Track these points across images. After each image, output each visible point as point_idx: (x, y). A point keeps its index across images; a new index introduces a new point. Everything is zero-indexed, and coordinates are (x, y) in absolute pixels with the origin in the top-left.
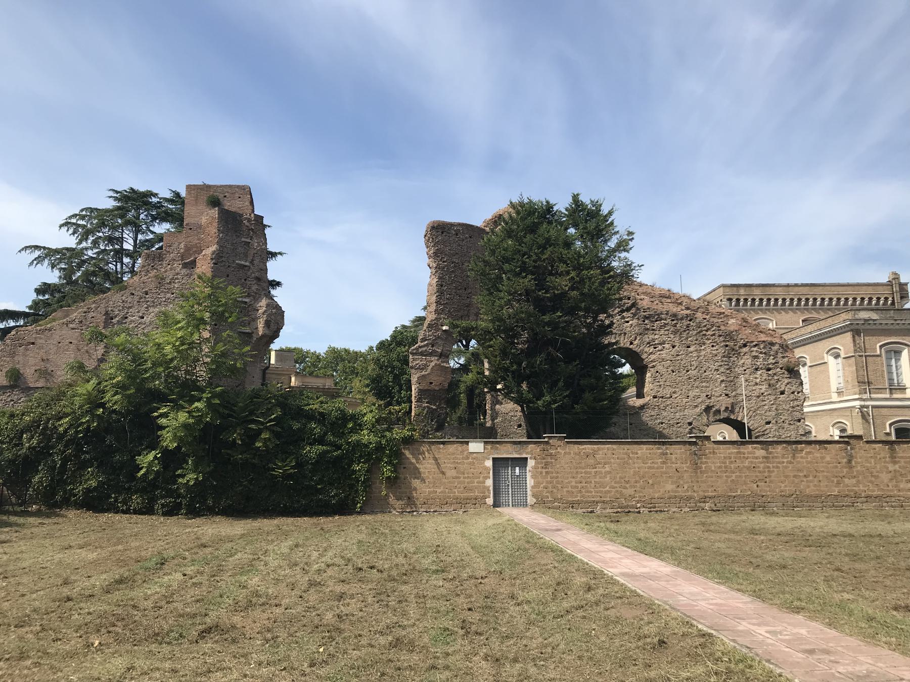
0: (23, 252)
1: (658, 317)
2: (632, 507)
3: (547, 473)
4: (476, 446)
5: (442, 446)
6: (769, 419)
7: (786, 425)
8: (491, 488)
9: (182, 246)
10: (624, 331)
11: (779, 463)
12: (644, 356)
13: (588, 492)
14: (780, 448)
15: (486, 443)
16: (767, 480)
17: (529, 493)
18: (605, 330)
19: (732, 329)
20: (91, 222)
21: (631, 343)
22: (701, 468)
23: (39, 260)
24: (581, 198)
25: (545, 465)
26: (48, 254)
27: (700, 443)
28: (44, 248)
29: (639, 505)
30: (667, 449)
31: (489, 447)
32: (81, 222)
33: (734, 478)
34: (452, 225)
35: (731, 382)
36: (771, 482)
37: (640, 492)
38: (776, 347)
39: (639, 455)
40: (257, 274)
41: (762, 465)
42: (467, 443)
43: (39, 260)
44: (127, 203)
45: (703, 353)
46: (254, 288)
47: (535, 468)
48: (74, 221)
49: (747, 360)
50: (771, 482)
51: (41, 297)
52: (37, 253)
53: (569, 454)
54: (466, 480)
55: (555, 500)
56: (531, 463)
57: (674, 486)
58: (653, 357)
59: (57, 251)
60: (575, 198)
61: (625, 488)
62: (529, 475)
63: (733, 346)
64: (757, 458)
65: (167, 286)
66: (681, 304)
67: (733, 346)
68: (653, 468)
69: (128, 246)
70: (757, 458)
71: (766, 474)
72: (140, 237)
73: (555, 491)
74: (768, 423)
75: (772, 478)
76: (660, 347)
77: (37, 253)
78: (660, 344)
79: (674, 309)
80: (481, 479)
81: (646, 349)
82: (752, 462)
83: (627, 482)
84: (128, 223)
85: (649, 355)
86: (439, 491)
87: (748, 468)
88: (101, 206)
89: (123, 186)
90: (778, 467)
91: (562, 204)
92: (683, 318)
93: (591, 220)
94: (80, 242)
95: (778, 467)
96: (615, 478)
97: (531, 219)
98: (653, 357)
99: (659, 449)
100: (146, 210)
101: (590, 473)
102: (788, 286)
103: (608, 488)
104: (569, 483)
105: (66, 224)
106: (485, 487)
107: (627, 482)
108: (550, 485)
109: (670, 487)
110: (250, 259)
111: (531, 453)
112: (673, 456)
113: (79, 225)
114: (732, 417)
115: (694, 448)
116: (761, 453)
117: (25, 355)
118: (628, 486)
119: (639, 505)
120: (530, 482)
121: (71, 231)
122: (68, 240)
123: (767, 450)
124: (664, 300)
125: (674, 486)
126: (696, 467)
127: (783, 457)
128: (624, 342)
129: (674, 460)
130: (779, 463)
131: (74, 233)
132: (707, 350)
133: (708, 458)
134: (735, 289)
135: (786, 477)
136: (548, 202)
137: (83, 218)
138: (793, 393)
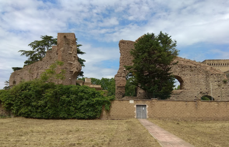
0: (19, 52)
1: (185, 67)
2: (177, 119)
3: (152, 109)
4: (132, 102)
5: (122, 101)
6: (219, 96)
7: (224, 97)
8: (136, 113)
9: (57, 49)
10: (174, 70)
11: (222, 107)
12: (182, 78)
13: (164, 115)
14: (222, 103)
15: (134, 100)
16: (218, 112)
17: (147, 115)
18: (169, 69)
19: (208, 70)
20: (35, 45)
21: (178, 74)
22: (198, 109)
23: (23, 54)
24: (162, 32)
25: (151, 107)
26: (26, 53)
27: (197, 101)
28: (25, 51)
29: (179, 119)
30: (187, 103)
31: (135, 102)
32: (34, 44)
33: (208, 112)
34: (126, 41)
35: (208, 85)
36: (219, 113)
37: (179, 115)
38: (221, 75)
39: (179, 105)
40: (74, 55)
41: (217, 108)
42: (129, 100)
43: (23, 54)
44: (45, 39)
45: (199, 77)
46: (74, 59)
47: (148, 108)
48: (32, 44)
49: (211, 79)
50: (219, 113)
51: (26, 64)
52: (23, 52)
53: (158, 104)
54: (129, 111)
55: (155, 117)
56: (147, 106)
57: (190, 114)
58: (184, 78)
59: (28, 52)
60: (161, 32)
61: (175, 114)
62: (147, 110)
63: (208, 75)
64: (215, 106)
65: (53, 59)
66: (192, 63)
67: (208, 75)
68: (183, 108)
69: (46, 51)
70: (215, 106)
71: (218, 111)
72: (49, 48)
73: (154, 114)
74: (219, 97)
75: (220, 112)
76: (187, 75)
77: (23, 52)
78: (187, 74)
79: (190, 65)
80: (133, 111)
81: (183, 76)
82: (214, 107)
83: (176, 112)
84: (46, 45)
85: (183, 78)
86: (121, 114)
87: (212, 109)
88: (39, 40)
89: (44, 35)
90: (221, 109)
91: (157, 34)
92: (193, 67)
93: (165, 39)
94: (33, 50)
95: (221, 109)
96: (172, 111)
97: (148, 39)
98: (184, 78)
99: (185, 103)
100: (50, 41)
101: (164, 109)
102: (225, 60)
103: (170, 114)
104: (159, 112)
105: (30, 45)
106: (134, 113)
107: (176, 112)
108: (153, 113)
109: (189, 114)
110: (72, 51)
111: (147, 103)
112: (189, 105)
113: (33, 45)
114: (208, 95)
115: (195, 103)
116: (216, 104)
117: (17, 78)
118: (176, 113)
119: (179, 119)
120: (147, 112)
121: (31, 46)
122: (30, 49)
123: (218, 103)
124: (188, 62)
125: (190, 114)
126: (196, 108)
127: (223, 106)
128: (176, 74)
129: (189, 106)
130: (222, 107)
131: (32, 47)
132: (200, 76)
133: (200, 106)
134: (209, 61)
135: (224, 111)
136: (153, 33)
137: (34, 43)
138: (226, 88)
